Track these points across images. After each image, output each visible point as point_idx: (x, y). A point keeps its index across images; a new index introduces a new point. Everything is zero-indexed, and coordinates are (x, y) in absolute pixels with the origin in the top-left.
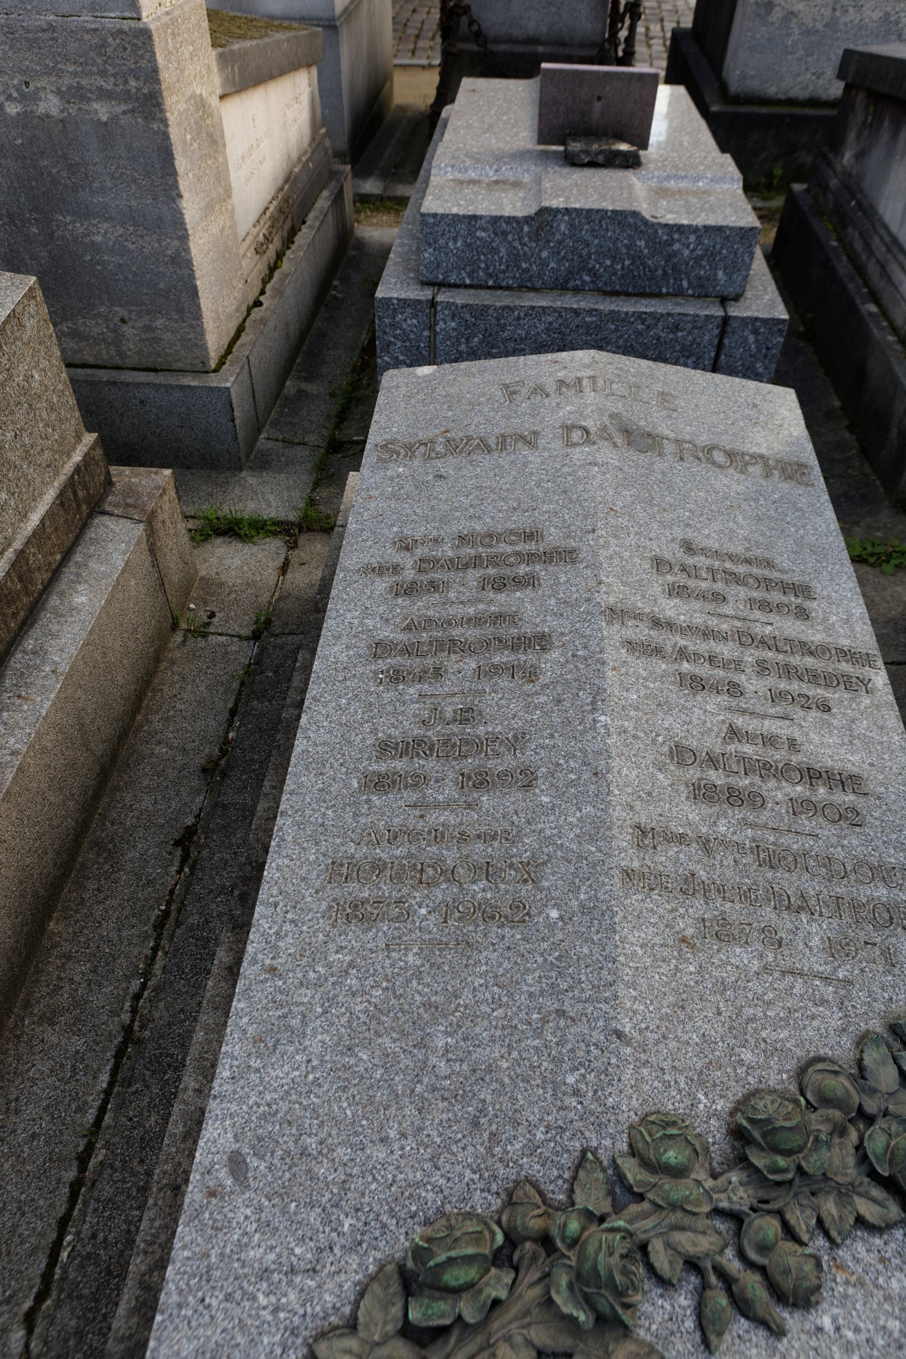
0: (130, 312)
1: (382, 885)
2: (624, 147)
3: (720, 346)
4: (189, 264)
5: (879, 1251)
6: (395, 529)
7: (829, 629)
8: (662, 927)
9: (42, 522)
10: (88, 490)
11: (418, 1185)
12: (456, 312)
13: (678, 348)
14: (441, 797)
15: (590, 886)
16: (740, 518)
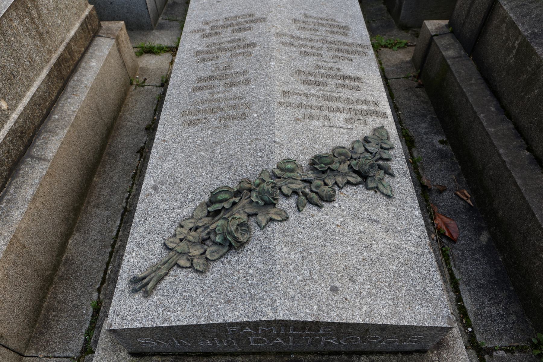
9: (75, 33)
10: (92, 26)
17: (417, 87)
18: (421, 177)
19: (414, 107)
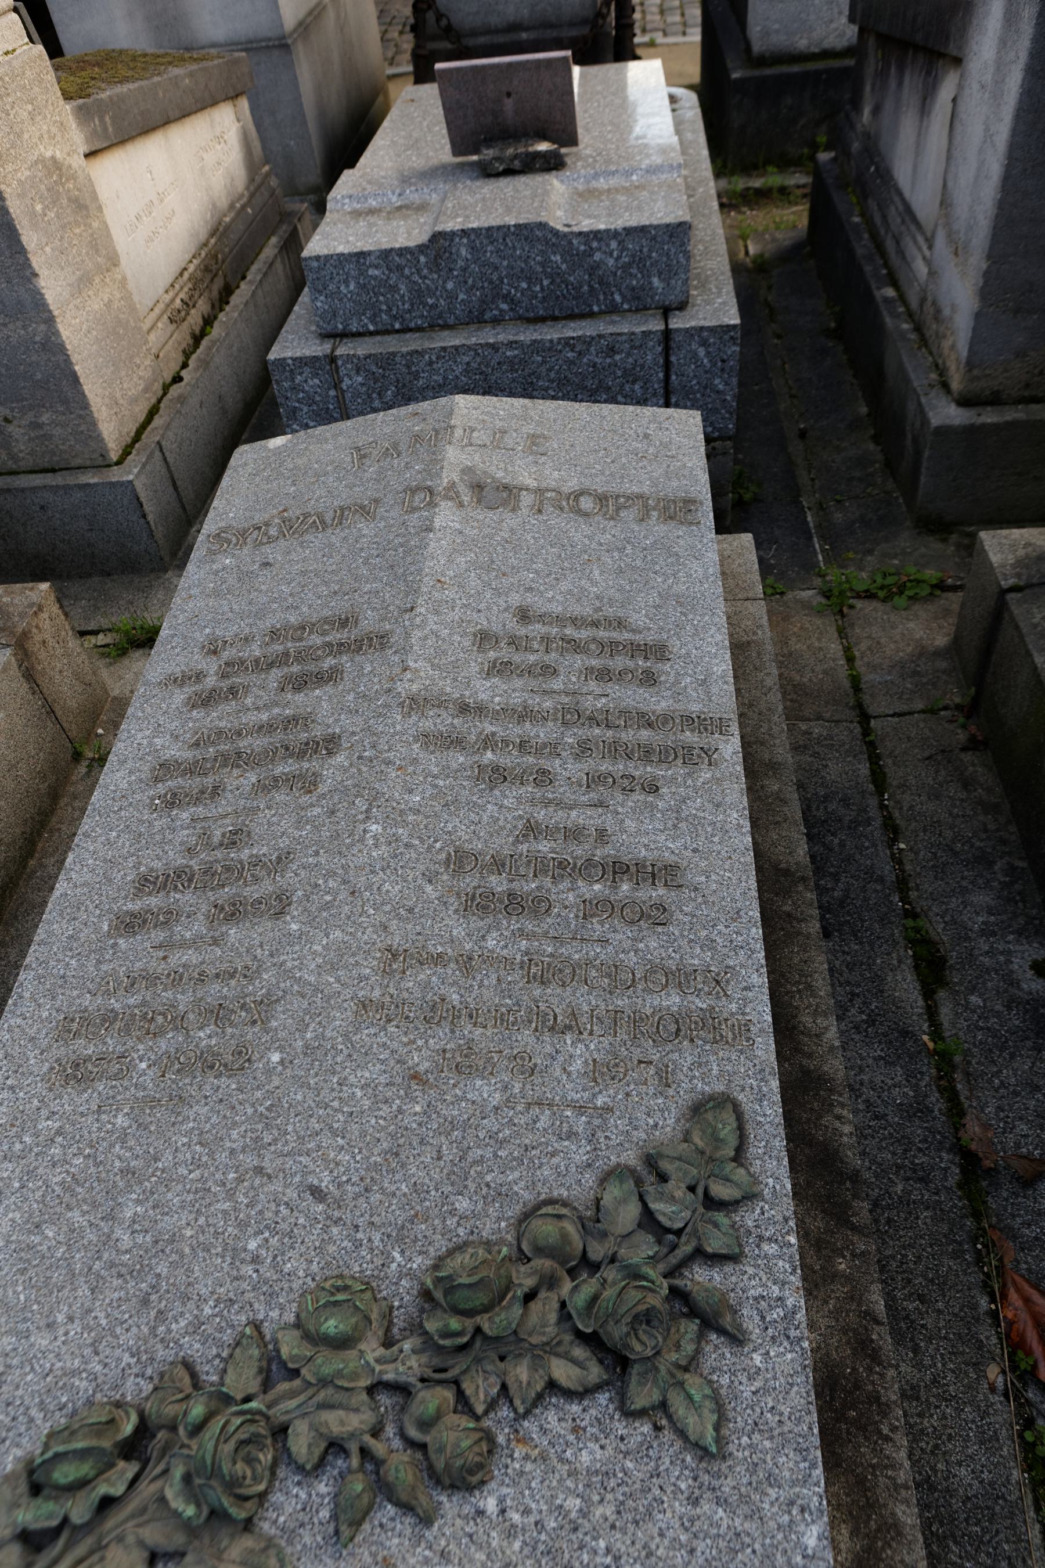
0: (12, 410)
1: (108, 1040)
2: (543, 147)
3: (667, 366)
4: (62, 348)
5: (574, 1420)
6: (207, 630)
7: (678, 695)
8: (392, 1063)
11: (74, 1373)
12: (359, 365)
13: (619, 373)
14: (188, 935)
15: (320, 1023)
16: (596, 573)
17: (964, 749)
18: (962, 1114)
19: (952, 827)
